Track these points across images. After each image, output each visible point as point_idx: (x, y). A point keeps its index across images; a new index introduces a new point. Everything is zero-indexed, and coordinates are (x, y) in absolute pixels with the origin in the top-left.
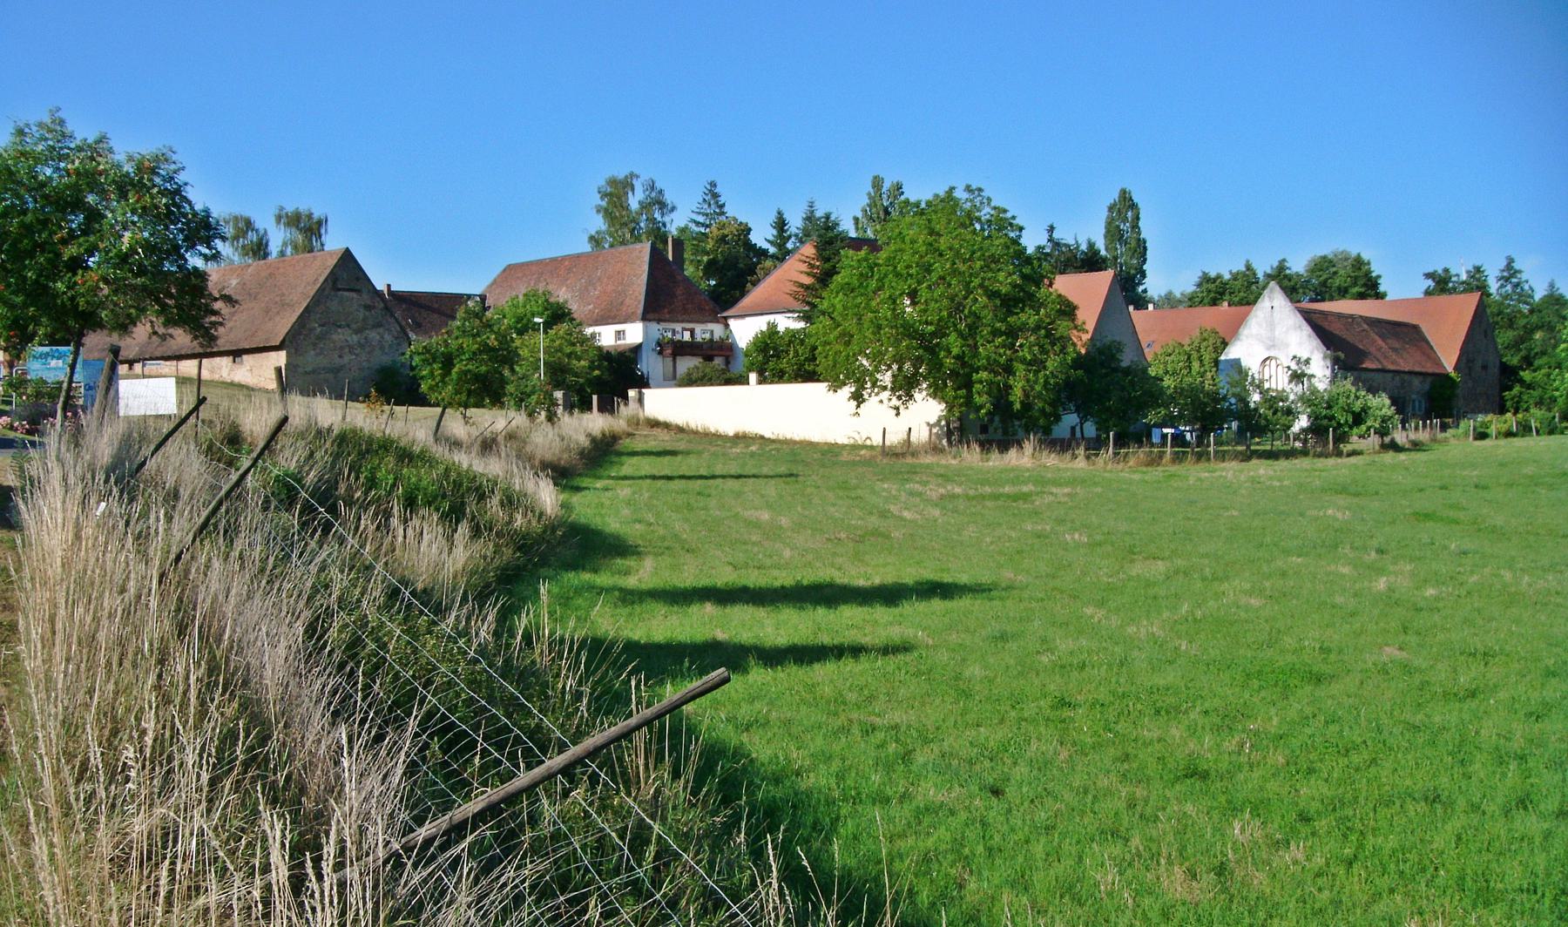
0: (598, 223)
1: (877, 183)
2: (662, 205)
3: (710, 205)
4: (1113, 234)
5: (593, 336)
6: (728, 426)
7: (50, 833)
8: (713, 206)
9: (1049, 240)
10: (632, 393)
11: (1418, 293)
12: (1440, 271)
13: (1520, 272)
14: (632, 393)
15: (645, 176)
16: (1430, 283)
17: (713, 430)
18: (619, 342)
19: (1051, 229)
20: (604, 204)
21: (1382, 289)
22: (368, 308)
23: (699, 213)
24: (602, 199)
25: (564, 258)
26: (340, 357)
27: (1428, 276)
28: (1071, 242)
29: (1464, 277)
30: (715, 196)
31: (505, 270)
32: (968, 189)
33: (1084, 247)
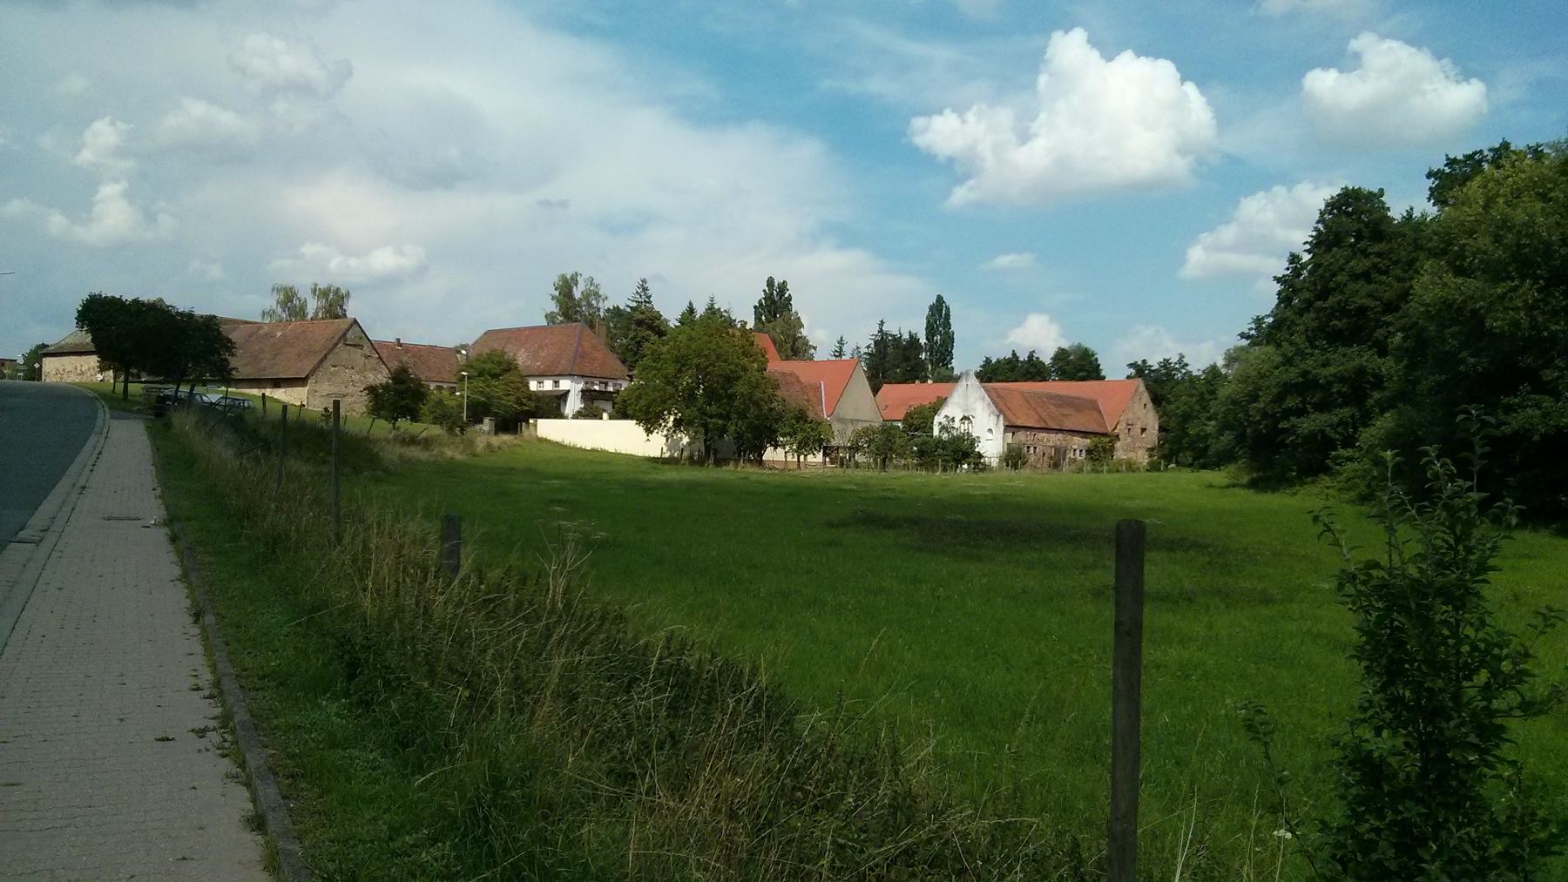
0: (553, 307)
1: (770, 282)
2: (597, 295)
3: (641, 296)
4: (931, 331)
5: (102, 369)
6: (588, 444)
7: (359, 812)
8: (643, 297)
9: (879, 332)
10: (531, 421)
11: (1123, 377)
12: (1140, 363)
13: (1187, 365)
14: (531, 421)
15: (586, 275)
16: (1132, 371)
17: (579, 446)
18: (557, 389)
19: (882, 323)
20: (557, 293)
21: (1103, 373)
22: (367, 357)
23: (633, 301)
24: (556, 289)
25: (525, 328)
26: (346, 387)
27: (1131, 365)
28: (895, 332)
29: (1156, 367)
30: (645, 289)
31: (485, 333)
32: (790, 295)
33: (906, 336)
